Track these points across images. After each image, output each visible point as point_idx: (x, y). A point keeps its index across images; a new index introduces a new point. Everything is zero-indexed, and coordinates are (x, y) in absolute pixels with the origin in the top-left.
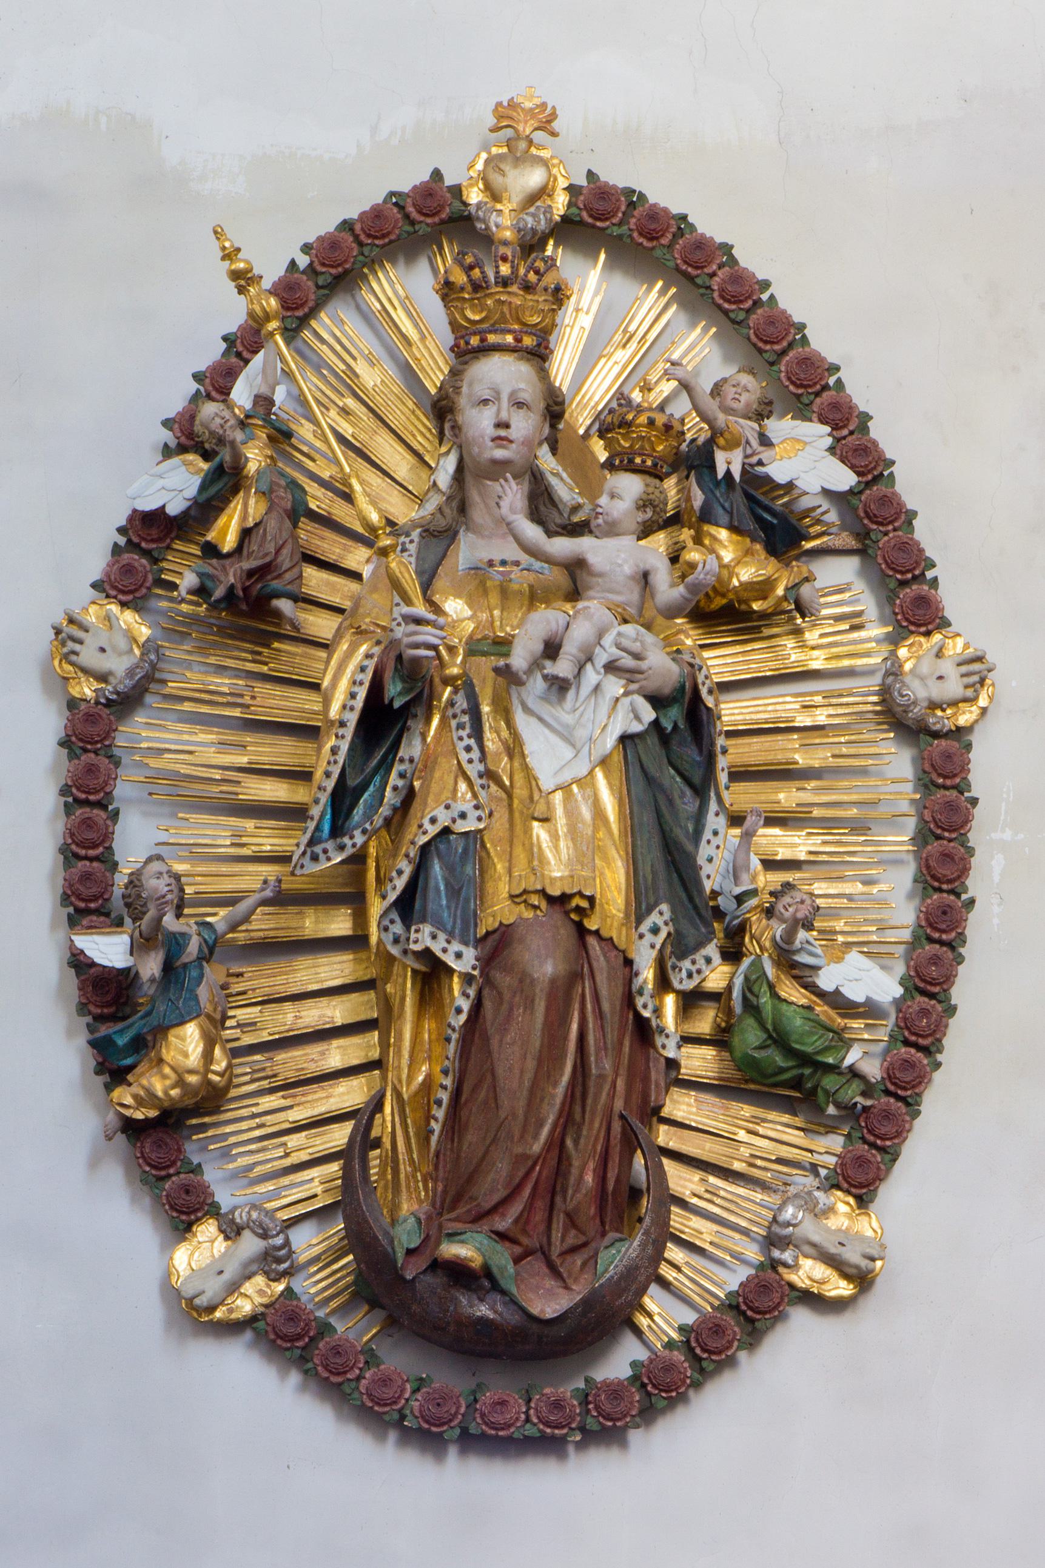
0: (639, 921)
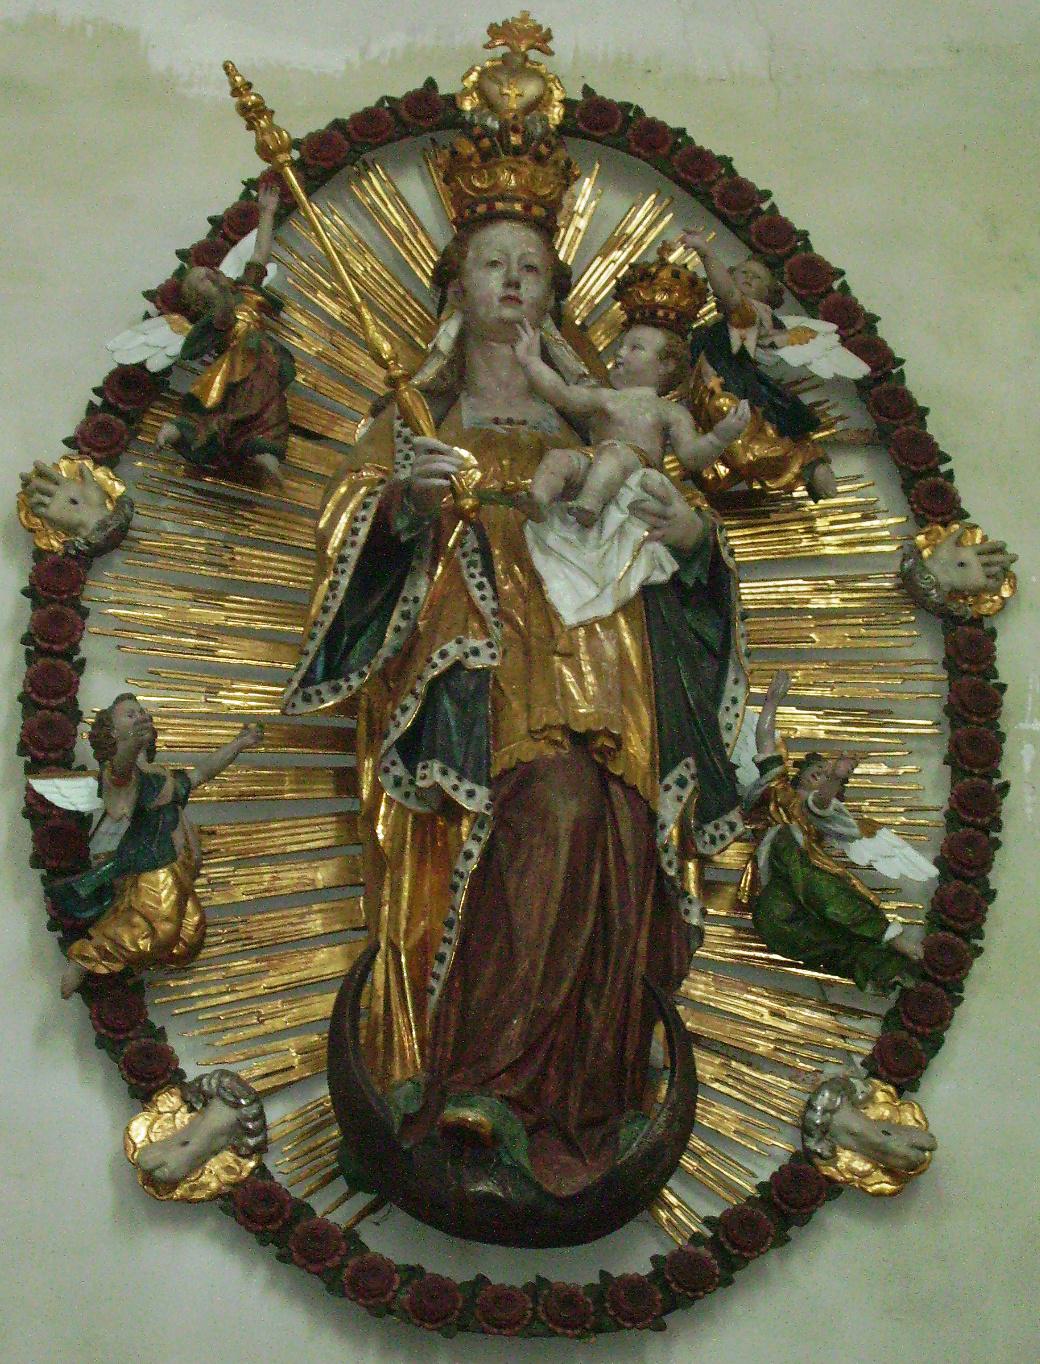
0: (664, 774)
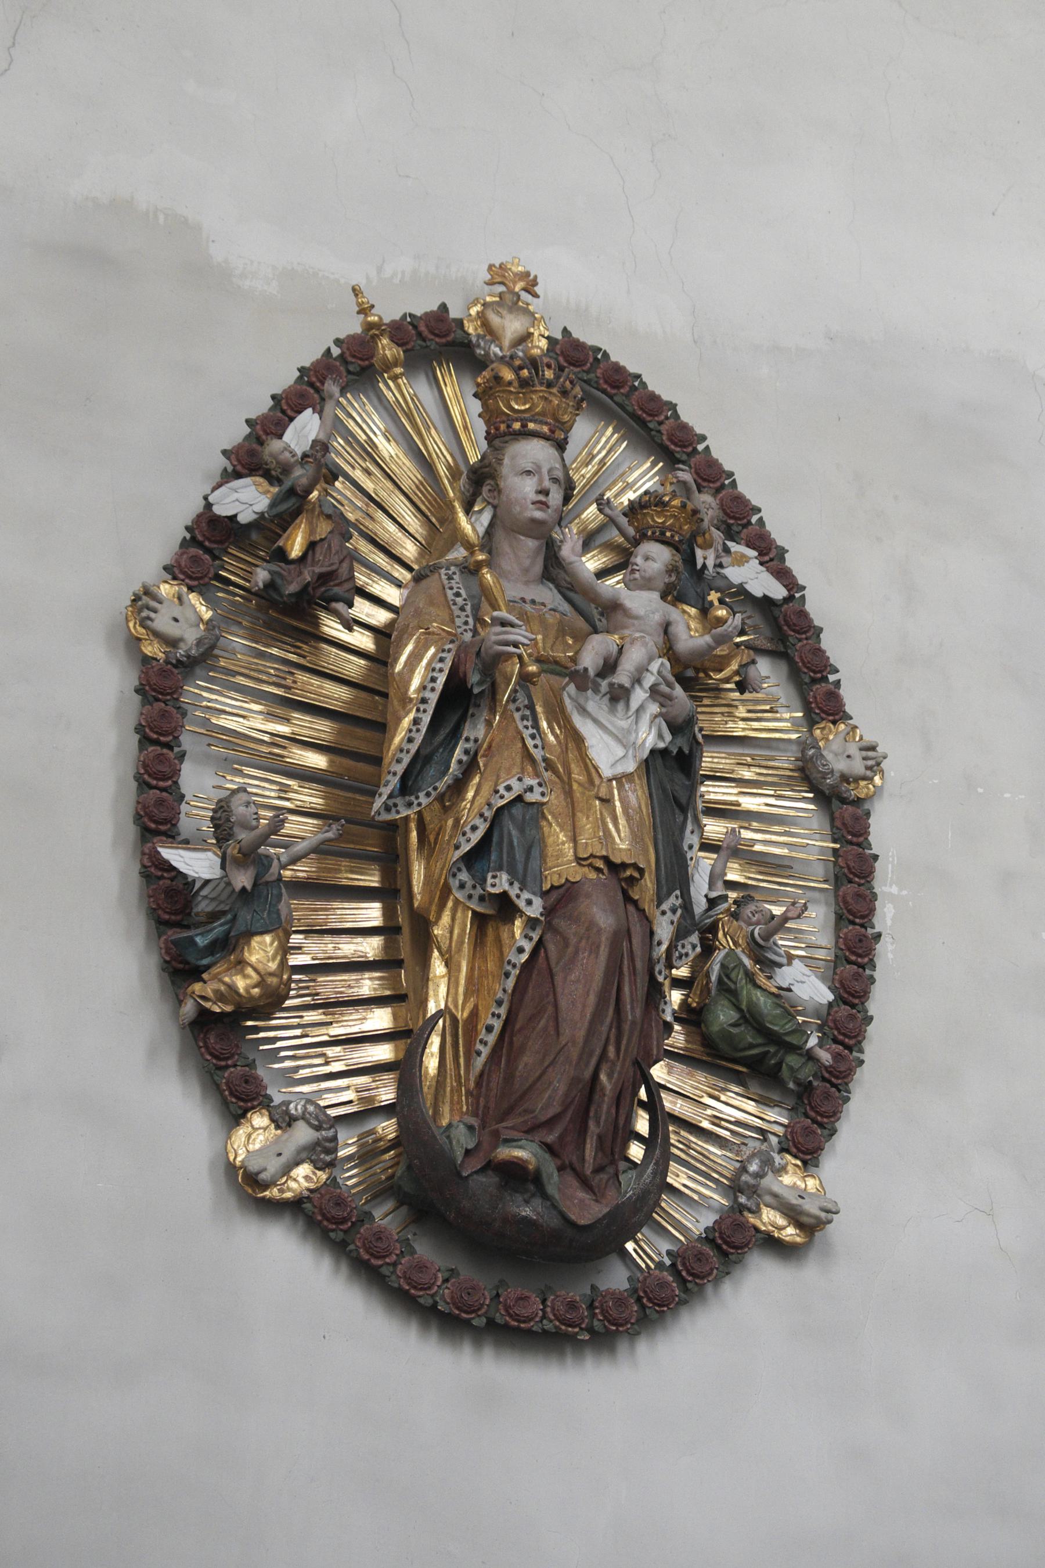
0: (659, 904)
